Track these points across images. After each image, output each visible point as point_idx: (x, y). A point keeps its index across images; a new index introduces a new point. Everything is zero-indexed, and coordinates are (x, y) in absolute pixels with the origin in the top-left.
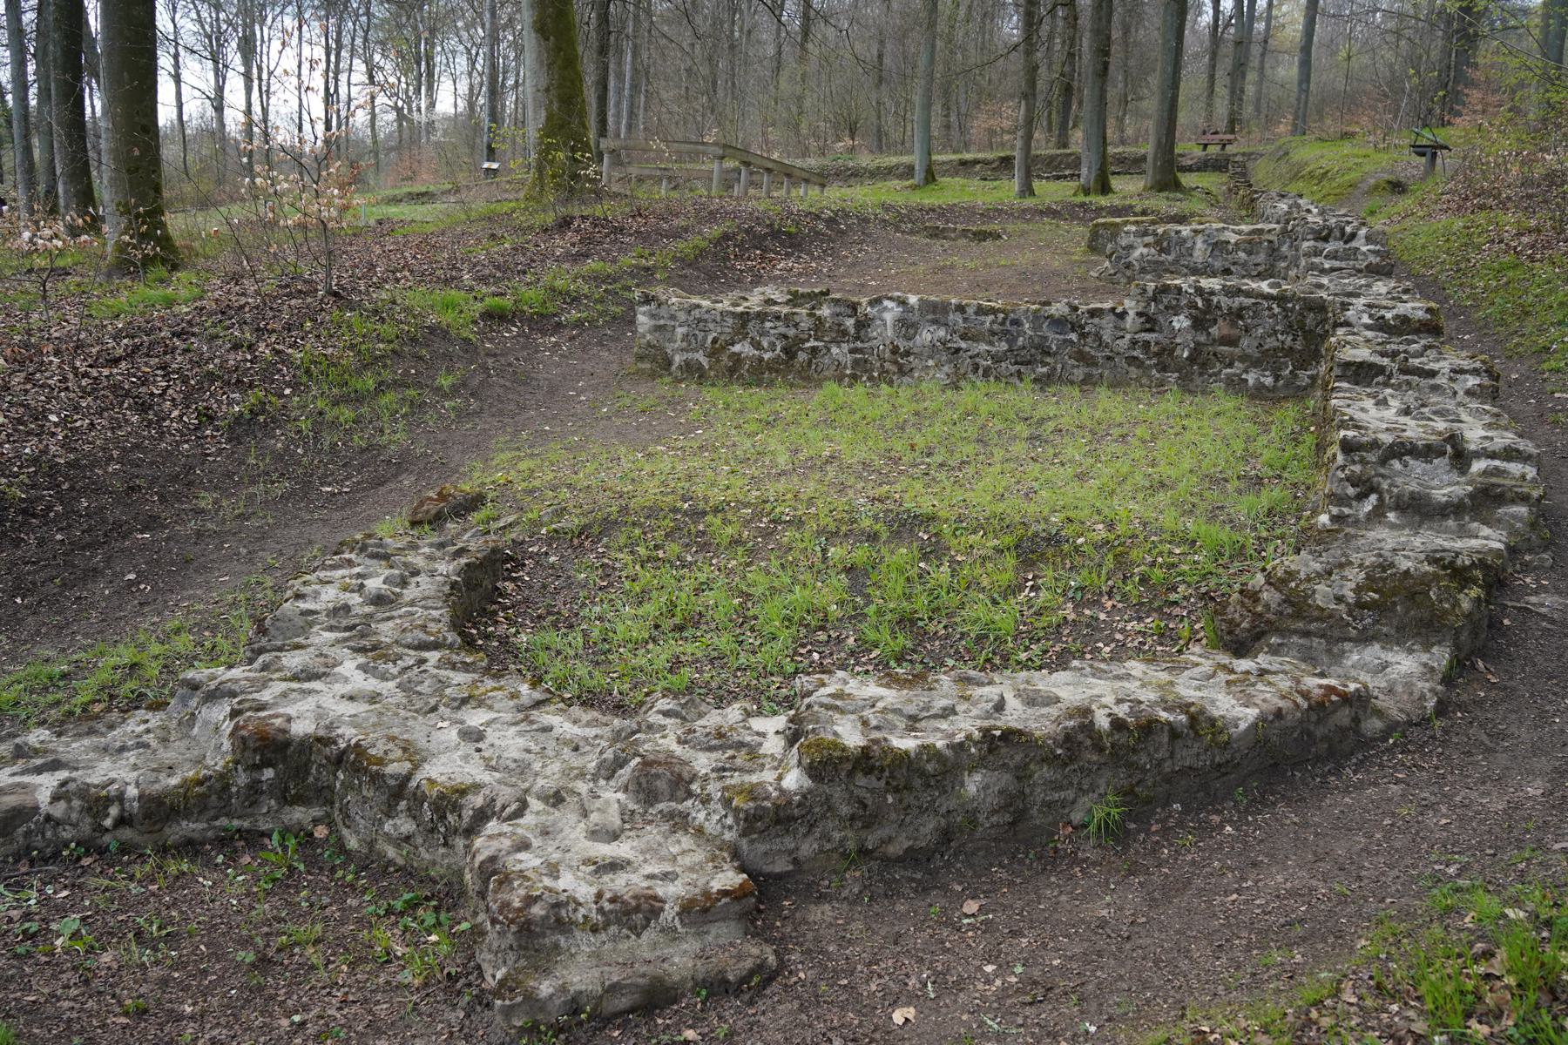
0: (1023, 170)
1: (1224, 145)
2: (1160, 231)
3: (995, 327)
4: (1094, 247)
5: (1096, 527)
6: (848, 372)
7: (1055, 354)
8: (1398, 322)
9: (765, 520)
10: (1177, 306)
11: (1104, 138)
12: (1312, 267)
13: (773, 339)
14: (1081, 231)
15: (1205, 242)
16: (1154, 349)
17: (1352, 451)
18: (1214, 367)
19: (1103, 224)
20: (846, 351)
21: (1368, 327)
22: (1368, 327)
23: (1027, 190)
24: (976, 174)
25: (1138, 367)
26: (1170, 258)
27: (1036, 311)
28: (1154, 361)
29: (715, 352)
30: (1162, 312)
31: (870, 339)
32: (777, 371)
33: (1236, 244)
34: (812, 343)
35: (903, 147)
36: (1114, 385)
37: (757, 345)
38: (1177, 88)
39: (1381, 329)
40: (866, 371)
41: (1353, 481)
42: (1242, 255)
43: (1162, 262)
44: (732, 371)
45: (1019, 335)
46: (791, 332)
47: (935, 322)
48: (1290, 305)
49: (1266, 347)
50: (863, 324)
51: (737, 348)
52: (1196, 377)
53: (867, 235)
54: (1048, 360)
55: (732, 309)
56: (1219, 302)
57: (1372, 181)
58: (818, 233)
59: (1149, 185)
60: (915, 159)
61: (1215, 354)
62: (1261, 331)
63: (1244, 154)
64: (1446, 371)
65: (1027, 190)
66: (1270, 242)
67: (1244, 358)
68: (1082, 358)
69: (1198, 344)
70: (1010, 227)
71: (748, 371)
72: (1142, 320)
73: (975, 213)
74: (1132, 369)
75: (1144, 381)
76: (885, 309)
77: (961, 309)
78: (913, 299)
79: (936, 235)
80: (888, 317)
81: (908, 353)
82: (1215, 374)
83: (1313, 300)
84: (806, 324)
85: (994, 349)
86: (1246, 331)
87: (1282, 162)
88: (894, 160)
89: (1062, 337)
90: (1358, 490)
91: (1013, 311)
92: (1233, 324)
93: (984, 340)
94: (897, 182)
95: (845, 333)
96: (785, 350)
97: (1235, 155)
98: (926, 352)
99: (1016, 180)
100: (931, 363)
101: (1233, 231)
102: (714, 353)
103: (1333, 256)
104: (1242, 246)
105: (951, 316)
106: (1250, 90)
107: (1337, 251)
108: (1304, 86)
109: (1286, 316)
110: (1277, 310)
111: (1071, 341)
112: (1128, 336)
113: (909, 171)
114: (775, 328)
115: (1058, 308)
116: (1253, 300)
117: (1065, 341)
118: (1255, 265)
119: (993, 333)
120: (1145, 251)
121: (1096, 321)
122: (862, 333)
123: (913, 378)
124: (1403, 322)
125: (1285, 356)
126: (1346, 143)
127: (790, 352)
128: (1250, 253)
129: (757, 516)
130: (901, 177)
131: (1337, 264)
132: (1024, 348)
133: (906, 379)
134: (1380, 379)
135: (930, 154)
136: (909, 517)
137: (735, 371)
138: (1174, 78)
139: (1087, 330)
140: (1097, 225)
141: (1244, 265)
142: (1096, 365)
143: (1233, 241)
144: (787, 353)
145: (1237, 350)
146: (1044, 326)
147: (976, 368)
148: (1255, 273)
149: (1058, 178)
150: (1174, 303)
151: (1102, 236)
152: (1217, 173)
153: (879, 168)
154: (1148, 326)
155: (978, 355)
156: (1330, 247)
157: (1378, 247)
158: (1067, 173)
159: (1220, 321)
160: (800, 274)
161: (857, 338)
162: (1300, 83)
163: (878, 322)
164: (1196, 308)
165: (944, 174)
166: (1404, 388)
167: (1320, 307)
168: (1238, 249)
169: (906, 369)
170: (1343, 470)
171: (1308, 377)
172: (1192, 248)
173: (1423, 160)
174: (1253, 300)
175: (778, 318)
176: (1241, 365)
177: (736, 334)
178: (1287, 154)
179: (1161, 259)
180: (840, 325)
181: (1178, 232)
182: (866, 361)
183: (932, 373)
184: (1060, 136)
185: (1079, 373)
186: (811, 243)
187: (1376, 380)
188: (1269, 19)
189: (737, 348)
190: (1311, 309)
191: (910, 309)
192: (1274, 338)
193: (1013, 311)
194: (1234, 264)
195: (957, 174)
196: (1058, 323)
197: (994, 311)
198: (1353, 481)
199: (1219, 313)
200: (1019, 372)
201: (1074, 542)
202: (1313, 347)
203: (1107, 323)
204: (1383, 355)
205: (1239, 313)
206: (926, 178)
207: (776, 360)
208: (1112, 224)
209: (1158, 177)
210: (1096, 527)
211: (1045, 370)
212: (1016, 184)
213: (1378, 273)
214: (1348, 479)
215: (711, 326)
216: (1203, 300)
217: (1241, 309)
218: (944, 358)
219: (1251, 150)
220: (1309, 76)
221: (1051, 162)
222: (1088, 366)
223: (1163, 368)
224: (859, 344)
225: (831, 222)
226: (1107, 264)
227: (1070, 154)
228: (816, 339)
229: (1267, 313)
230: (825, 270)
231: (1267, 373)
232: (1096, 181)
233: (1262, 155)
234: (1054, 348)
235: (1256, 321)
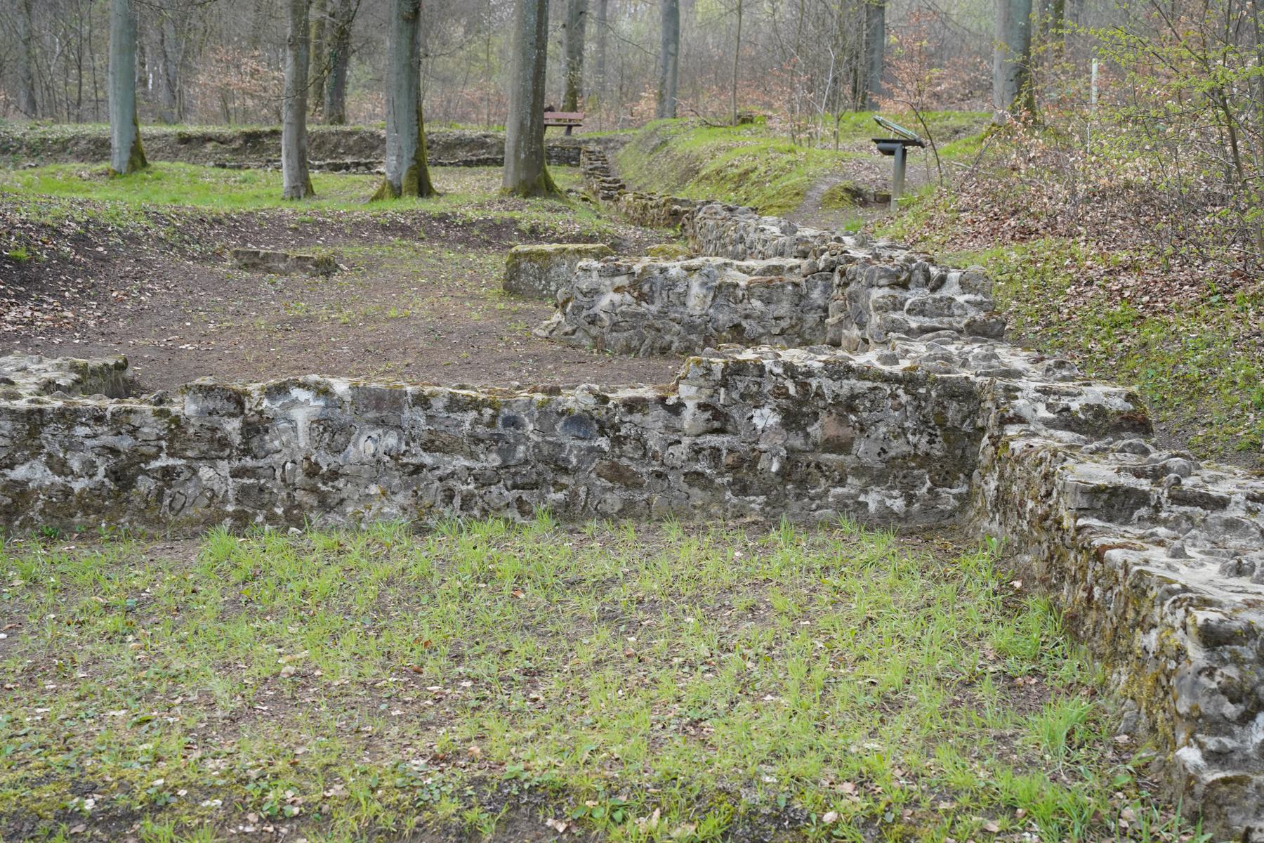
1: (570, 127)
2: (637, 268)
3: (480, 430)
4: (512, 287)
5: (840, 789)
6: (230, 508)
8: (1090, 416)
9: (252, 817)
10: (759, 393)
11: (419, 113)
12: (894, 326)
13: (90, 455)
14: (494, 263)
15: (704, 284)
16: (727, 459)
17: (1219, 644)
18: (818, 485)
19: (527, 254)
21: (1048, 424)
24: (208, 157)
25: (704, 488)
26: (654, 308)
27: (542, 405)
28: (728, 478)
30: (736, 403)
31: (268, 453)
32: (98, 511)
33: (748, 288)
34: (164, 461)
35: (78, 109)
36: (682, 514)
37: (60, 467)
39: (1067, 426)
40: (262, 506)
41: (1232, 693)
42: (757, 304)
43: (644, 315)
45: (518, 442)
46: (125, 443)
47: (380, 423)
48: (922, 391)
49: (892, 453)
50: (256, 428)
51: (20, 473)
52: (791, 501)
53: (144, 263)
54: (565, 480)
56: (820, 387)
57: (825, 188)
58: (64, 260)
59: (510, 186)
60: (110, 128)
61: (818, 466)
62: (883, 429)
63: (598, 141)
64: (1240, 497)
65: (302, 188)
66: (796, 285)
67: (860, 471)
68: (618, 475)
69: (791, 450)
70: (348, 252)
71: (42, 512)
73: (283, 228)
74: (696, 491)
75: (714, 509)
76: (295, 402)
77: (422, 401)
78: (341, 386)
79: (254, 265)
81: (334, 475)
82: (819, 497)
83: (957, 383)
84: (152, 428)
85: (477, 465)
86: (862, 430)
88: (69, 129)
89: (585, 444)
90: (1242, 707)
91: (507, 404)
92: (842, 420)
93: (461, 451)
95: (223, 443)
96: (114, 474)
98: (366, 472)
100: (374, 489)
101: (740, 269)
103: (919, 310)
104: (757, 291)
105: (407, 414)
106: (590, 47)
107: (924, 303)
108: (671, 48)
110: (904, 398)
111: (601, 451)
112: (686, 441)
113: (100, 148)
114: (95, 436)
115: (577, 399)
116: (869, 384)
117: (591, 450)
118: (776, 319)
119: (477, 440)
120: (617, 297)
121: (637, 417)
122: (255, 443)
123: (344, 515)
124: (1096, 416)
125: (920, 467)
127: (122, 477)
128: (767, 302)
129: (235, 810)
130: (81, 156)
131: (927, 322)
132: (526, 462)
133: (332, 518)
134: (1144, 511)
135: (135, 124)
136: (521, 791)
137: (17, 513)
139: (623, 432)
140: (517, 255)
142: (639, 486)
143: (743, 284)
144: (117, 480)
145: (849, 458)
147: (449, 496)
148: (778, 331)
149: (336, 168)
150: (754, 388)
152: (566, 167)
153: (44, 141)
154: (716, 424)
156: (914, 296)
157: (979, 298)
158: (349, 160)
159: (823, 415)
160: (49, 331)
161: (246, 452)
162: (666, 44)
163: (283, 425)
164: (788, 396)
166: (1184, 525)
167: (966, 394)
168: (751, 295)
169: (333, 500)
170: (1211, 675)
172: (685, 294)
173: (890, 159)
174: (869, 384)
175: (99, 419)
181: (663, 270)
182: (261, 490)
183: (375, 506)
184: (332, 104)
185: (614, 501)
187: (1136, 514)
189: (20, 473)
190: (952, 396)
192: (902, 440)
193: (507, 404)
194: (747, 317)
195: (175, 156)
196: (578, 422)
197: (476, 405)
198: (1232, 693)
199: (821, 404)
200: (519, 500)
201: (820, 820)
202: (959, 452)
203: (654, 421)
205: (849, 404)
206: (132, 162)
208: (540, 254)
209: (522, 176)
210: (840, 789)
211: (560, 496)
212: (284, 179)
213: (984, 334)
217: (853, 397)
218: (396, 481)
220: (676, 33)
222: (628, 487)
223: (744, 490)
224: (249, 462)
225: (80, 241)
226: (557, 316)
227: (351, 134)
228: (171, 455)
229: (890, 402)
230: (92, 323)
231: (895, 493)
232: (410, 176)
233: (623, 144)
234: (574, 461)
235: (875, 415)
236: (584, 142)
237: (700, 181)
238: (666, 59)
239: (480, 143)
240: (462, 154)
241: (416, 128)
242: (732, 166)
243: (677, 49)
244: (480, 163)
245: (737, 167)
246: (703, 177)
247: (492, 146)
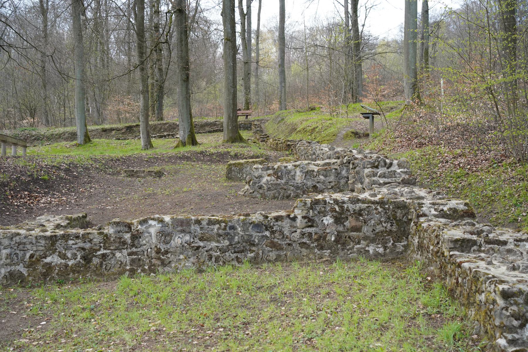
0: (145, 133)
1: (247, 116)
3: (220, 231)
6: (128, 268)
7: (258, 245)
8: (451, 212)
10: (325, 211)
11: (191, 114)
13: (75, 251)
14: (222, 168)
15: (301, 171)
16: (315, 237)
17: (509, 297)
19: (234, 164)
20: (126, 254)
21: (436, 216)
22: (436, 216)
23: (149, 145)
24: (113, 136)
26: (283, 181)
27: (243, 220)
29: (32, 264)
31: (141, 246)
33: (318, 171)
34: (102, 251)
37: (63, 256)
38: (236, 87)
40: (140, 266)
42: (322, 177)
43: (279, 184)
44: (45, 275)
45: (235, 235)
46: (88, 246)
47: (183, 231)
48: (387, 206)
49: (377, 231)
50: (136, 237)
51: (48, 260)
52: (340, 251)
54: (254, 248)
55: (42, 234)
56: (348, 207)
58: (62, 178)
59: (226, 139)
60: (77, 128)
62: (373, 222)
63: (258, 120)
65: (149, 145)
66: (336, 169)
67: (365, 238)
68: (274, 245)
69: (339, 232)
70: (167, 168)
71: (57, 274)
72: (306, 220)
75: (311, 256)
77: (198, 222)
78: (167, 218)
79: (132, 175)
80: (153, 231)
81: (167, 252)
82: (351, 249)
85: (220, 245)
86: (365, 223)
88: (61, 130)
89: (260, 234)
90: (520, 322)
91: (230, 221)
92: (357, 219)
93: (214, 240)
94: (65, 143)
95: (124, 243)
96: (84, 258)
97: (253, 121)
99: (142, 139)
100: (182, 257)
101: (314, 165)
102: (31, 265)
103: (383, 176)
104: (321, 173)
105: (193, 227)
106: (253, 86)
107: (385, 173)
108: (283, 84)
109: (386, 212)
110: (380, 210)
112: (299, 231)
113: (73, 136)
114: (76, 244)
116: (366, 205)
117: (263, 236)
118: (329, 182)
119: (220, 235)
120: (269, 178)
121: (279, 223)
124: (454, 212)
125: (388, 235)
126: (311, 112)
127: (87, 259)
128: (326, 176)
130: (66, 139)
131: (386, 180)
132: (239, 242)
134: (475, 248)
135: (86, 126)
137: (48, 275)
138: (233, 82)
139: (274, 229)
140: (230, 165)
141: (323, 183)
142: (282, 249)
143: (316, 170)
144: (85, 260)
145: (361, 234)
146: (250, 228)
147: (210, 257)
149: (161, 137)
150: (323, 209)
151: (234, 170)
152: (246, 131)
153: (52, 135)
154: (310, 224)
155: (211, 249)
156: (381, 171)
157: (406, 170)
158: (165, 134)
159: (350, 218)
160: (57, 205)
161: (133, 246)
162: (281, 83)
163: (146, 235)
164: (336, 211)
165: (94, 136)
168: (320, 174)
169: (166, 262)
171: (402, 246)
172: (295, 175)
173: (368, 120)
174: (366, 205)
175: (77, 237)
176: (364, 242)
177: (47, 250)
179: (278, 182)
180: (120, 238)
181: (286, 167)
185: (273, 255)
186: (59, 185)
187: (472, 249)
188: (258, 49)
189: (48, 260)
190: (398, 208)
191: (167, 225)
192: (380, 226)
193: (230, 221)
194: (318, 182)
196: (257, 226)
197: (218, 222)
199: (349, 213)
202: (402, 229)
203: (286, 224)
204: (472, 233)
205: (359, 213)
206: (85, 140)
207: (78, 265)
208: (239, 164)
209: (230, 135)
211: (252, 255)
212: (142, 142)
214: (512, 316)
215: (29, 247)
216: (339, 206)
217: (361, 210)
218: (190, 253)
219: (261, 118)
220: (284, 79)
222: (278, 250)
223: (322, 248)
224: (134, 249)
226: (247, 187)
227: (166, 124)
228: (105, 249)
229: (375, 211)
230: (73, 201)
231: (379, 246)
232: (189, 138)
233: (267, 121)
234: (257, 241)
235: (370, 217)
239: (214, 124)
240: (207, 129)
243: (285, 85)
247: (219, 125)
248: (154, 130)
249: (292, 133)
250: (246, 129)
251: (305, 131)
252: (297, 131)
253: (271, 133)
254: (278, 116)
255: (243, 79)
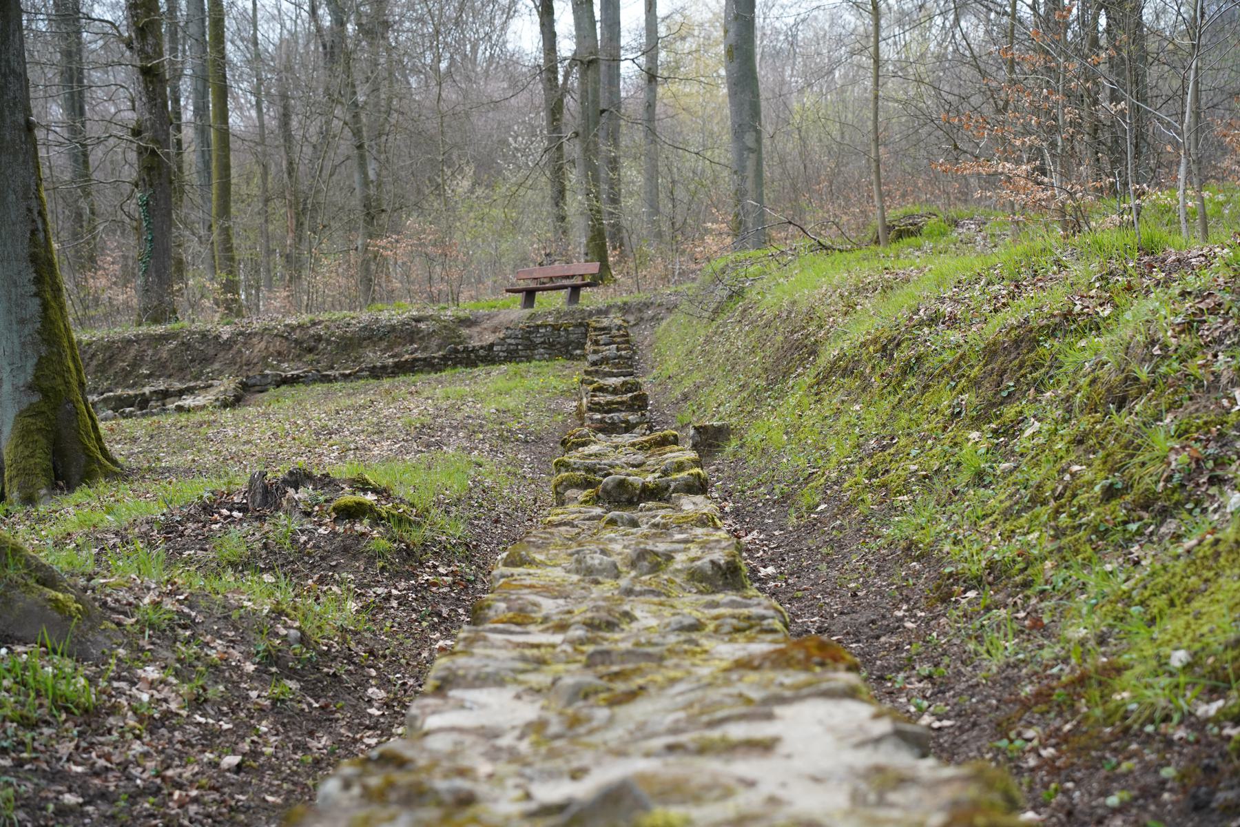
1: (575, 290)
63: (625, 309)
87: (730, 318)
108: (749, 139)
162: (738, 133)
178: (737, 294)
220: (755, 112)
221: (111, 360)
232: (24, 435)
236: (600, 312)
237: (823, 379)
238: (741, 160)
239: (408, 333)
240: (373, 356)
241: (34, 305)
242: (933, 320)
243: (758, 140)
244: (403, 368)
245: (953, 321)
246: (833, 368)
247: (431, 335)
248: (102, 369)
249: (786, 375)
250: (561, 354)
251: (907, 369)
252: (823, 361)
253: (672, 371)
254: (717, 278)
255: (577, 134)
